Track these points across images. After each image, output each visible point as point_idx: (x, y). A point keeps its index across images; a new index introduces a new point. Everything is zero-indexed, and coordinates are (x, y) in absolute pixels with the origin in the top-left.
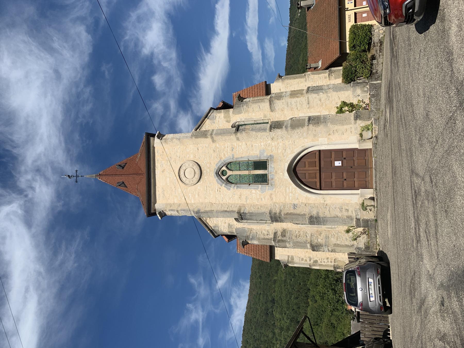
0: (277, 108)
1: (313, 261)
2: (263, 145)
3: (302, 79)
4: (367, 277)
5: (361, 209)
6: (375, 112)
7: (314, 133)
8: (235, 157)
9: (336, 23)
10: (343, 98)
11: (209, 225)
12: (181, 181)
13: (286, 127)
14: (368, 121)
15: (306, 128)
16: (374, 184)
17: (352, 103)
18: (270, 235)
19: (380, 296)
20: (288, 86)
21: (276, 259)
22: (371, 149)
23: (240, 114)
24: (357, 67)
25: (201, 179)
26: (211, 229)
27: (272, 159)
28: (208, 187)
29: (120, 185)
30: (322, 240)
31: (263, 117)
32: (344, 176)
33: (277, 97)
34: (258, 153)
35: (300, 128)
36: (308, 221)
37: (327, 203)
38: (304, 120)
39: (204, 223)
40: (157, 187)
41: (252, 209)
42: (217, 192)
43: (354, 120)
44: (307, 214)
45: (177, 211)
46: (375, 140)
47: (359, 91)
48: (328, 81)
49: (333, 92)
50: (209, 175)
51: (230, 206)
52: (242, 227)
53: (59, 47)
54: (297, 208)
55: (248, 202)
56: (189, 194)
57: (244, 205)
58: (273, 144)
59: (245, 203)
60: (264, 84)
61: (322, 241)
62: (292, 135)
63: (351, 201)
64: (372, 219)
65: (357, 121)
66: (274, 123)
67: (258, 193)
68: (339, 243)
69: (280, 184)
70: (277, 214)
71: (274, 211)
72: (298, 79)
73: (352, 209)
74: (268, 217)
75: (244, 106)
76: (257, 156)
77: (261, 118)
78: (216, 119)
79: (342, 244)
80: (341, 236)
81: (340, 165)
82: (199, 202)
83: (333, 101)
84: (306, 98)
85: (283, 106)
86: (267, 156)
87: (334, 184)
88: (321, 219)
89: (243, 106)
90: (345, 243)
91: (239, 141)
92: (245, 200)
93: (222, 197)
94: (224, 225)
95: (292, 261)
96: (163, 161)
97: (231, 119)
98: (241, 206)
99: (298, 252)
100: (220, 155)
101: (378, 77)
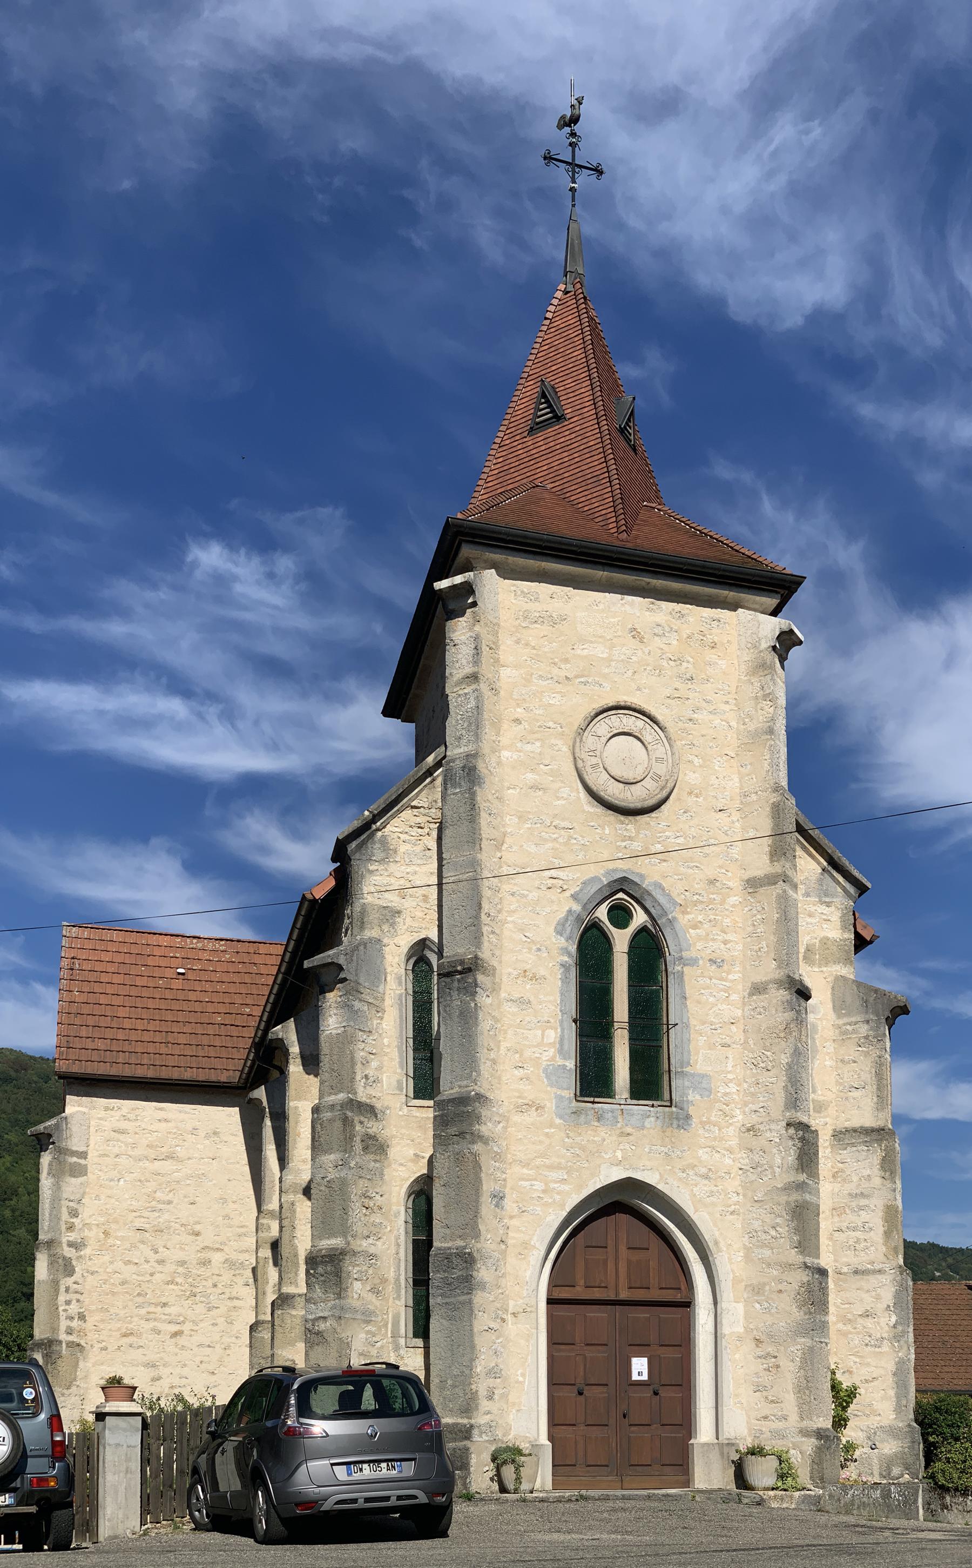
0: (845, 1154)
2: (728, 1091)
4: (417, 1456)
7: (767, 1288)
8: (686, 969)
9: (955, 1382)
10: (866, 1393)
11: (393, 817)
12: (597, 715)
14: (811, 1477)
15: (794, 1256)
18: (365, 1087)
19: (357, 1499)
21: (67, 1101)
22: (687, 1483)
23: (834, 1007)
25: (600, 810)
26: (374, 827)
27: (675, 1122)
28: (570, 837)
29: (547, 402)
31: (816, 1098)
36: (449, 1248)
39: (400, 795)
43: (818, 1429)
45: (474, 678)
46: (750, 1497)
47: (890, 1447)
52: (389, 969)
53: (772, 147)
55: (510, 1009)
56: (538, 744)
57: (495, 989)
58: (731, 1131)
59: (503, 995)
61: (356, 1296)
67: (546, 1053)
69: (580, 1149)
74: (460, 1087)
75: (866, 1027)
76: (689, 1064)
78: (822, 903)
81: (635, 1377)
82: (506, 784)
83: (858, 1360)
84: (881, 1266)
86: (688, 1101)
88: (462, 1298)
89: (868, 1022)
91: (746, 994)
92: (516, 995)
93: (527, 893)
95: (67, 1168)
96: (675, 642)
98: (494, 975)
99: (103, 1197)
100: (695, 903)
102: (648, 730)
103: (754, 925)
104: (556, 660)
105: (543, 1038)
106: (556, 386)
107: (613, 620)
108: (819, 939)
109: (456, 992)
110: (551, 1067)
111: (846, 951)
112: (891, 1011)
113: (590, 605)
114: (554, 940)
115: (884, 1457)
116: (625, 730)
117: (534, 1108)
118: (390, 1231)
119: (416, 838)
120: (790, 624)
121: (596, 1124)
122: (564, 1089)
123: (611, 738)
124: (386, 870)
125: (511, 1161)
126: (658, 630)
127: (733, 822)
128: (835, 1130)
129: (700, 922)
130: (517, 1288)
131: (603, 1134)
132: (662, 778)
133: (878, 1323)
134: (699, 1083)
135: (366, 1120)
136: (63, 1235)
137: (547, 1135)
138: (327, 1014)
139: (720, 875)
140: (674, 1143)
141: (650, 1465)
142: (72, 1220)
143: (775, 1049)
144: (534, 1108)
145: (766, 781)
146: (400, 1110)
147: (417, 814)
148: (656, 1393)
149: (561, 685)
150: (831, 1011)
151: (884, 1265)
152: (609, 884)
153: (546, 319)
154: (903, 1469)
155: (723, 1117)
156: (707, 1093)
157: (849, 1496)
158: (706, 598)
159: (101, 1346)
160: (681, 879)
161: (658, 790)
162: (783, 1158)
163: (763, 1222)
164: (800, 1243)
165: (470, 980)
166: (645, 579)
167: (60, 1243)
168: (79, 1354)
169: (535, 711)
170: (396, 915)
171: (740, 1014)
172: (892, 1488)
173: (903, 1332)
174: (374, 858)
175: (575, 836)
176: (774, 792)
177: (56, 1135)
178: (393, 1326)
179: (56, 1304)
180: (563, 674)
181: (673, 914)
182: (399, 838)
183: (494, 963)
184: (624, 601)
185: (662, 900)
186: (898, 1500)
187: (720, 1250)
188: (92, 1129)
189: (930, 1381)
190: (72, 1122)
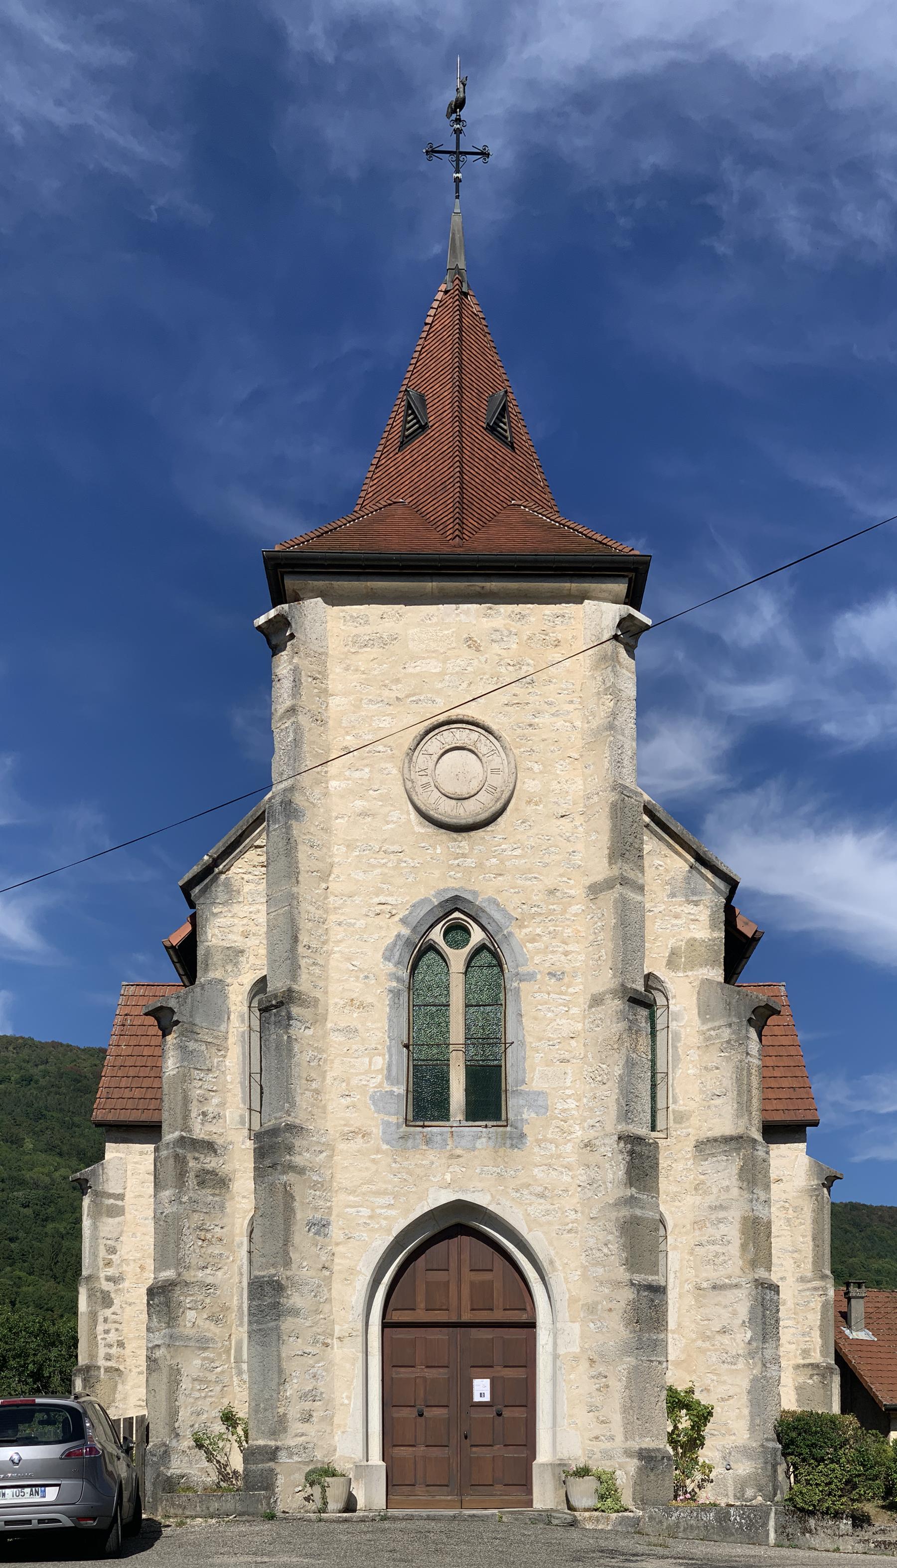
1: (107, 1289)
2: (566, 1107)
3: (809, 1266)
4: (64, 1482)
5: (311, 1467)
7: (600, 1307)
8: (523, 985)
10: (722, 1412)
11: (236, 858)
12: (427, 733)
13: (631, 1201)
14: (634, 1499)
15: (622, 1274)
16: (404, 1513)
17: (703, 1444)
18: (202, 1124)
20: (790, 1211)
22: (530, 1503)
24: (832, 1466)
25: (431, 829)
26: (216, 870)
27: (508, 1142)
28: (400, 861)
31: (676, 1108)
34: (534, 1084)
36: (264, 1277)
37: (332, 1348)
38: (656, 1269)
40: (401, 608)
43: (641, 1449)
44: (289, 1273)
45: (292, 710)
47: (744, 1468)
48: (792, 1362)
49: (751, 1377)
50: (451, 867)
52: (233, 1008)
54: (311, 1234)
56: (367, 770)
57: (320, 1019)
58: (569, 1147)
59: (329, 1025)
60: (809, 1116)
61: (189, 1325)
63: (343, 1432)
64: (275, 1502)
65: (636, 1461)
66: (650, 1151)
67: (374, 1080)
68: (183, 1387)
69: (407, 1173)
70: (288, 1157)
71: (298, 1142)
72: (814, 1250)
73: (313, 1434)
74: (276, 1118)
75: (728, 1031)
76: (523, 1082)
77: (675, 1102)
78: (689, 902)
80: (210, 1394)
81: (477, 1398)
82: (334, 814)
83: (715, 1378)
84: (738, 1280)
85: (715, 1190)
86: (522, 1120)
88: (273, 1324)
89: (730, 1025)
90: (186, 1408)
92: (342, 1025)
93: (353, 921)
94: (235, 929)
95: (104, 1209)
96: (515, 646)
97: (681, 975)
98: (316, 1006)
99: (138, 1235)
101: (788, 1535)
102: (483, 741)
103: (595, 933)
104: (387, 682)
105: (370, 1065)
106: (423, 392)
107: (446, 632)
108: (685, 941)
109: (273, 1026)
110: (378, 1094)
113: (422, 620)
114: (381, 966)
115: (738, 1478)
116: (458, 745)
117: (360, 1136)
118: (233, 1261)
119: (260, 877)
120: (628, 610)
121: (424, 1147)
123: (443, 755)
124: (230, 911)
125: (337, 1188)
127: (576, 827)
128: (697, 1141)
129: (538, 935)
130: (342, 1312)
131: (431, 1157)
133: (735, 1340)
134: (535, 1101)
135: (203, 1156)
136: (100, 1270)
137: (373, 1161)
138: (167, 1057)
139: (561, 884)
140: (507, 1163)
141: (492, 1485)
142: (110, 1257)
144: (360, 1136)
145: (606, 780)
146: (243, 1144)
147: (261, 853)
148: (499, 1415)
149: (391, 707)
150: (697, 1017)
152: (441, 905)
153: (426, 324)
155: (560, 1134)
156: (543, 1110)
158: (549, 594)
159: (138, 1370)
160: (519, 892)
161: (493, 802)
162: (614, 1173)
165: (284, 1014)
166: (477, 584)
167: (98, 1278)
168: (117, 1378)
170: (240, 954)
171: (580, 1028)
172: (732, 1511)
173: (757, 1348)
174: (218, 901)
175: (404, 859)
176: (612, 791)
177: (92, 1180)
178: (236, 1352)
179: (95, 1333)
180: (393, 695)
181: (509, 929)
182: (243, 879)
183: (318, 994)
185: (497, 916)
187: (555, 1269)
188: (129, 1173)
190: (109, 1167)
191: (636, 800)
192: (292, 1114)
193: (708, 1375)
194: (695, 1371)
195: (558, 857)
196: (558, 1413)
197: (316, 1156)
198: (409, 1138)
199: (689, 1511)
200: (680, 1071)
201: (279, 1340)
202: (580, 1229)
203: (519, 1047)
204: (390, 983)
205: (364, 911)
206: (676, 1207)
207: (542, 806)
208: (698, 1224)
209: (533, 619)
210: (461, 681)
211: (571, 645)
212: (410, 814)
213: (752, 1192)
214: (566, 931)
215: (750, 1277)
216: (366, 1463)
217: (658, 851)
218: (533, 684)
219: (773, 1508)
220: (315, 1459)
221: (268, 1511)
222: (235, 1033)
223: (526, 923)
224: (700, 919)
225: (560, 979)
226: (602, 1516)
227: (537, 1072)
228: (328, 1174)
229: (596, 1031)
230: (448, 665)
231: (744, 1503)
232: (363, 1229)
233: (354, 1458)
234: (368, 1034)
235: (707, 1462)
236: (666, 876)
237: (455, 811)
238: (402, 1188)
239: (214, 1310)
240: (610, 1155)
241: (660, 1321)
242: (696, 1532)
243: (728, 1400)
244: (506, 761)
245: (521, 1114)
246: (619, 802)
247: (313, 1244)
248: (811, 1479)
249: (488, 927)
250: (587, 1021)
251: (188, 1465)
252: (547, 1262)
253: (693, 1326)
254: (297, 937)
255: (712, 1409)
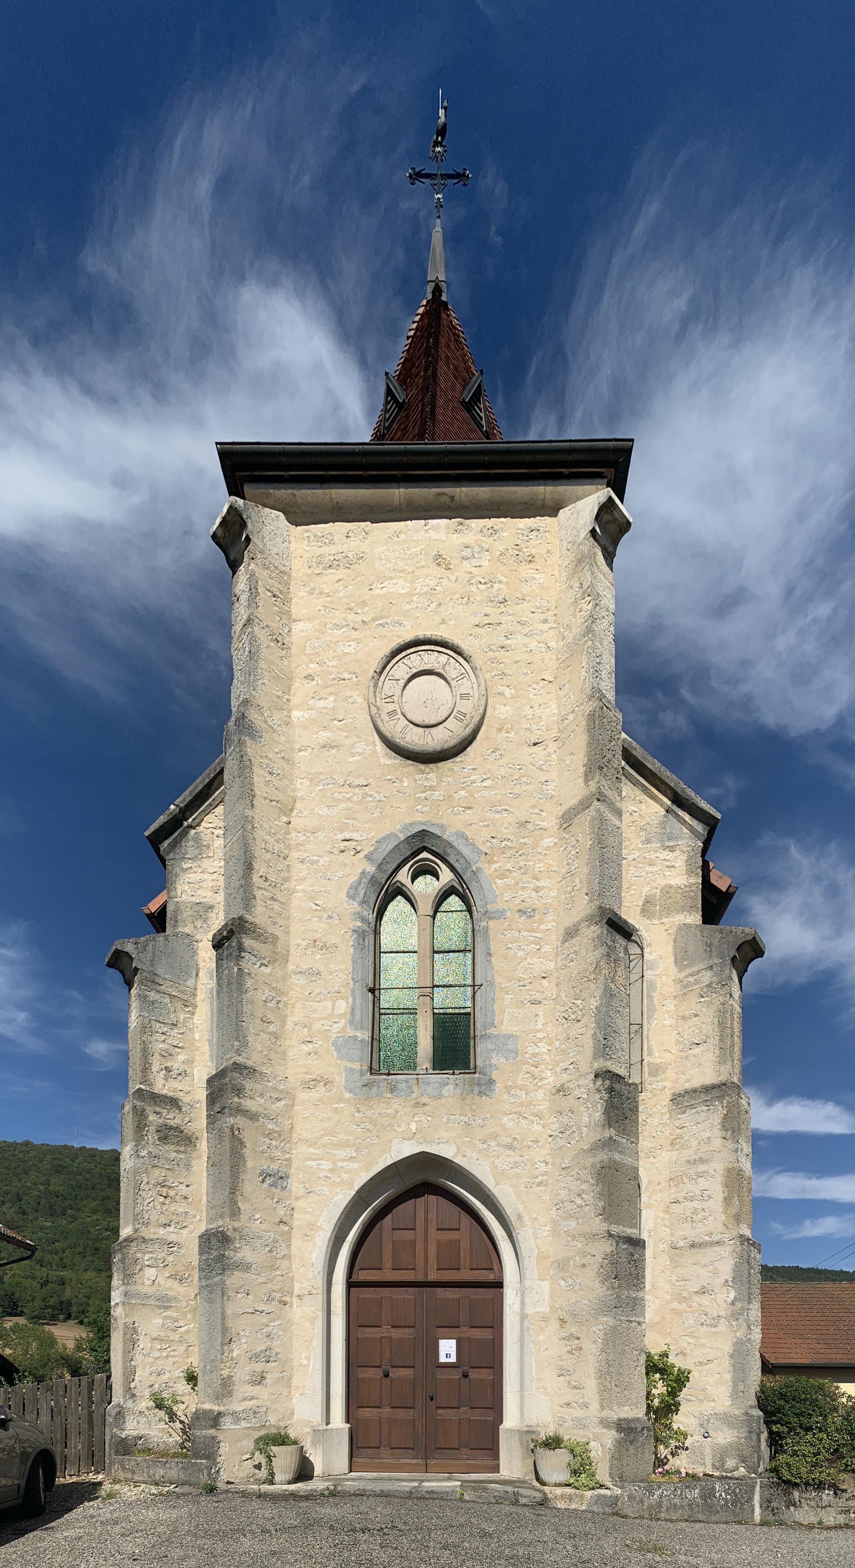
0: (685, 1118)
2: (537, 1051)
5: (263, 1432)
6: (645, 1499)
7: (572, 1263)
8: (491, 923)
10: (700, 1377)
13: (608, 1144)
14: (610, 1474)
15: (598, 1225)
17: (677, 1410)
18: (166, 1079)
22: (496, 1469)
24: (821, 1435)
25: (398, 761)
27: (477, 1089)
30: (150, 1282)
31: (652, 1060)
32: (400, 1369)
33: (739, 1113)
34: (503, 1027)
35: (601, 1204)
37: (291, 1306)
38: (634, 1221)
41: (259, 992)
42: (341, 837)
43: (620, 1420)
44: (236, 1224)
46: (529, 1497)
47: (724, 1436)
49: (735, 1340)
51: (276, 891)
52: (202, 965)
54: (265, 1185)
55: (298, 981)
56: (331, 699)
57: (279, 958)
58: (540, 1094)
59: (291, 967)
61: (147, 1283)
62: (574, 1173)
64: (218, 1472)
66: (630, 1092)
67: (337, 1025)
68: (141, 1347)
69: (371, 1123)
70: (236, 1099)
71: (249, 1085)
73: (266, 1397)
74: (227, 1060)
76: (492, 1025)
77: (650, 1054)
78: (665, 848)
79: (138, 1359)
80: (172, 1353)
81: (443, 1359)
82: (297, 746)
86: (491, 1065)
87: (370, 1333)
88: (218, 1279)
89: (711, 967)
90: (144, 1368)
91: (559, 944)
92: (305, 967)
93: (316, 858)
94: (204, 884)
97: (656, 922)
101: (773, 1510)
102: (452, 664)
105: (333, 1009)
107: (415, 550)
108: (660, 888)
109: (225, 961)
110: (341, 1039)
111: (691, 897)
112: (738, 949)
113: (390, 538)
114: (346, 905)
115: (717, 1446)
117: (322, 1084)
120: (609, 492)
121: (389, 1095)
122: (355, 1061)
124: (200, 866)
126: (467, 553)
127: (549, 755)
129: (508, 870)
131: (396, 1105)
132: (468, 716)
133: (715, 1300)
134: (504, 1045)
135: (165, 1111)
139: (533, 816)
141: (458, 1449)
143: (585, 995)
144: (322, 1084)
151: (722, 1235)
154: (738, 1461)
155: (531, 1080)
157: (655, 1497)
158: (522, 506)
160: (488, 825)
161: (462, 729)
163: (569, 1191)
164: (604, 1209)
169: (328, 663)
170: (210, 910)
171: (552, 967)
173: (742, 1309)
174: (187, 856)
175: (370, 793)
180: (359, 618)
181: (478, 865)
182: (213, 833)
183: (278, 932)
184: (428, 527)
185: (465, 850)
186: (726, 1500)
187: (523, 1225)
189: (841, 1356)
191: (614, 715)
192: (243, 1054)
193: (684, 1338)
194: (669, 1334)
195: (529, 787)
196: (526, 1377)
197: (273, 1103)
198: (373, 1085)
199: (673, 1489)
200: (656, 1021)
201: (223, 1296)
202: (550, 1182)
203: (488, 988)
204: (354, 923)
205: (328, 847)
206: (651, 1163)
207: (513, 733)
208: (675, 1180)
209: (505, 534)
210: (430, 602)
211: (546, 560)
212: (376, 745)
213: (738, 1142)
214: (537, 865)
215: (735, 1233)
216: (325, 1427)
217: (633, 797)
218: (506, 604)
219: (758, 1481)
220: (268, 1424)
221: (209, 1482)
222: (204, 989)
223: (495, 858)
224: (676, 865)
225: (531, 916)
226: (575, 1494)
227: (507, 1013)
228: (287, 1124)
229: (569, 967)
230: (417, 585)
231: (725, 1474)
232: (324, 1183)
233: (313, 1422)
234: (331, 977)
235: (682, 1428)
236: (641, 822)
237: (422, 739)
238: (364, 1140)
239: (177, 1268)
240: (585, 1096)
241: (640, 1277)
242: (680, 1512)
243: (707, 1364)
244: (476, 684)
245: (490, 1058)
246: (597, 710)
247: (268, 1196)
248: (799, 1450)
249: (457, 866)
250: (560, 958)
251: (147, 1426)
252: (515, 1217)
253: (668, 1287)
254: (251, 864)
255: (689, 1373)
